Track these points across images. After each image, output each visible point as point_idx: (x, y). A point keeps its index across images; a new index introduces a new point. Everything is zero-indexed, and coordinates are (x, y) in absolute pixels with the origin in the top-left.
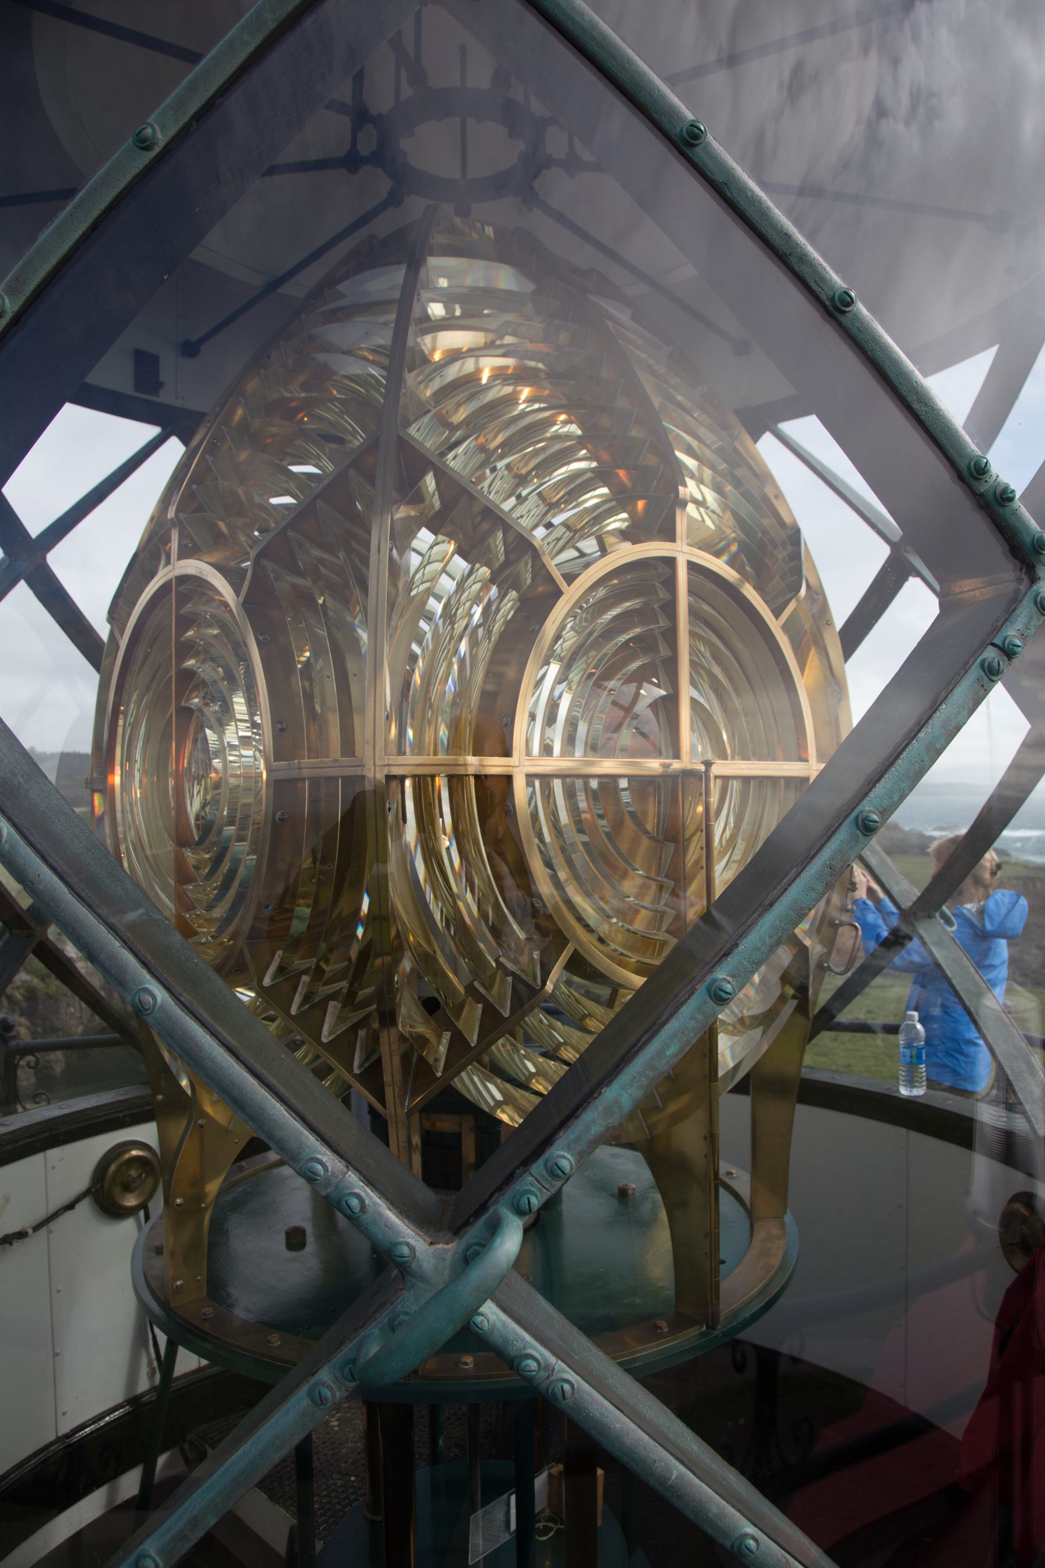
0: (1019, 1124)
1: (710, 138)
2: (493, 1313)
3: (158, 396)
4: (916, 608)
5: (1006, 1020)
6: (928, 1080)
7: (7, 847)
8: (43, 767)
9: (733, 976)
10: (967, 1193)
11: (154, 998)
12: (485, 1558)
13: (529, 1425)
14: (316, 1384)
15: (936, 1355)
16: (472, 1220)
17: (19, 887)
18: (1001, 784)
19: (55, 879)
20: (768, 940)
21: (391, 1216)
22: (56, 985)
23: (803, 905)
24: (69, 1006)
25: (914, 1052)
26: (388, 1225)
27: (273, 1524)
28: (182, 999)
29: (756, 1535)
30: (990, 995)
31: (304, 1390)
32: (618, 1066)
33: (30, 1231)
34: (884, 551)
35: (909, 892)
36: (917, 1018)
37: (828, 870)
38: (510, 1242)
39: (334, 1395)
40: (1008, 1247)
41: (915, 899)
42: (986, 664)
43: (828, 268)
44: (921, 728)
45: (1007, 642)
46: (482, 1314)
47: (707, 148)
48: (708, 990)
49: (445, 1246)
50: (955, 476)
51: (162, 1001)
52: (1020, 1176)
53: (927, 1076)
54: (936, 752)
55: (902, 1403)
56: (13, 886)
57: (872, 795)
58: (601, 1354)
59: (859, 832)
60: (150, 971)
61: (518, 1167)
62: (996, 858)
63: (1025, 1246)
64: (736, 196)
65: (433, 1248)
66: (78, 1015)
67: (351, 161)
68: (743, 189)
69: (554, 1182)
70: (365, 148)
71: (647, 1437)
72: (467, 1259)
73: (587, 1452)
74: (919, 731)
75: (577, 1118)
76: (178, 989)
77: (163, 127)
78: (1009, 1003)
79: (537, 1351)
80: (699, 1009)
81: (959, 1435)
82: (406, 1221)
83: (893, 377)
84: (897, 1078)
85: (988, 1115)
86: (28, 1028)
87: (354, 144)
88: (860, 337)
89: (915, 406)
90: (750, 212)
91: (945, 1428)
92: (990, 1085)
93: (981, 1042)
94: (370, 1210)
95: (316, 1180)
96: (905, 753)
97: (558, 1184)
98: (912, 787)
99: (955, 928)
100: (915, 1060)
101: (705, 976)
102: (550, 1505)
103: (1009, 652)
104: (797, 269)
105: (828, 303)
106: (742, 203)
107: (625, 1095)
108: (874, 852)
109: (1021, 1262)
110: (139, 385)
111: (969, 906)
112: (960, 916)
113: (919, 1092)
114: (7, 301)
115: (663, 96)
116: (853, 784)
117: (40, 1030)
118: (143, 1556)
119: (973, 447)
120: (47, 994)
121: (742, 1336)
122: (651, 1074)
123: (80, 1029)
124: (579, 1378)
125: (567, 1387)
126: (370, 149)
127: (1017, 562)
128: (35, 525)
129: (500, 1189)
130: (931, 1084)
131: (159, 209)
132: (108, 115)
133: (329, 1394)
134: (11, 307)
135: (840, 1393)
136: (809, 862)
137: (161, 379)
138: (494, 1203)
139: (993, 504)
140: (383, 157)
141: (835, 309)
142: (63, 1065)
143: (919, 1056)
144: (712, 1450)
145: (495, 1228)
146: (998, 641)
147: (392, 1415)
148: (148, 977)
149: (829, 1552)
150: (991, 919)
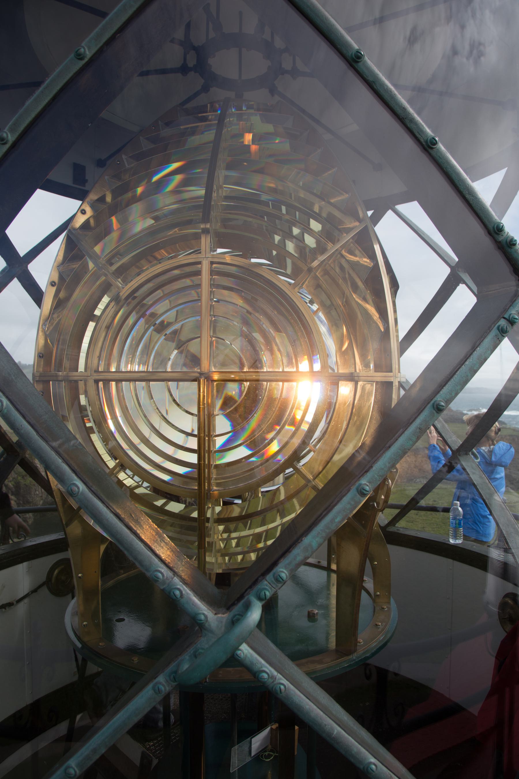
0: (510, 559)
1: (366, 58)
2: (246, 649)
3: (84, 186)
4: (463, 301)
6: (464, 535)
7: (5, 411)
8: (25, 371)
9: (370, 482)
10: (484, 592)
11: (78, 488)
13: (261, 704)
14: (156, 683)
15: (466, 673)
16: (236, 602)
17: (12, 431)
19: (29, 428)
21: (196, 600)
22: (29, 480)
23: (406, 447)
24: (36, 491)
25: (457, 522)
27: (134, 751)
28: (92, 489)
29: (376, 763)
30: (496, 494)
31: (151, 686)
33: (15, 603)
34: (447, 270)
35: (456, 442)
36: (459, 505)
37: (418, 430)
38: (255, 614)
39: (165, 689)
41: (459, 445)
42: (500, 328)
43: (425, 126)
46: (240, 650)
47: (365, 63)
48: (357, 489)
49: (223, 616)
50: (487, 233)
53: (463, 534)
54: (474, 372)
56: (6, 427)
57: (441, 392)
59: (434, 411)
61: (259, 577)
62: (498, 425)
63: (511, 620)
65: (216, 616)
66: (40, 495)
67: (184, 69)
68: (383, 85)
69: (278, 584)
70: (192, 62)
71: (322, 713)
72: (234, 622)
73: (290, 719)
74: (466, 361)
75: (290, 552)
76: (90, 484)
77: (89, 48)
78: (505, 498)
79: (268, 669)
81: (476, 713)
82: (203, 603)
83: (456, 181)
84: (448, 535)
85: (495, 554)
86: (15, 501)
87: (185, 59)
89: (467, 196)
90: (386, 96)
91: (471, 710)
95: (158, 581)
96: (458, 372)
97: (280, 585)
99: (479, 460)
100: (457, 526)
101: (356, 482)
103: (512, 322)
104: (409, 126)
105: (424, 144)
106: (382, 92)
107: (314, 541)
109: (509, 627)
110: (75, 181)
111: (483, 448)
112: (480, 453)
113: (459, 541)
115: (343, 37)
117: (21, 502)
118: (69, 767)
119: (496, 218)
120: (25, 484)
121: (369, 661)
122: (327, 531)
123: (41, 502)
124: (288, 683)
125: (282, 687)
126: (196, 62)
128: (22, 251)
129: (250, 587)
130: (466, 538)
131: (97, 78)
133: (163, 688)
135: (418, 691)
136: (409, 426)
137: (87, 178)
139: (505, 246)
140: (201, 67)
141: (428, 147)
142: (32, 520)
143: (460, 524)
144: (354, 720)
145: (248, 607)
146: (506, 316)
147: (192, 698)
148: (75, 477)
149: (412, 770)
150: (495, 455)
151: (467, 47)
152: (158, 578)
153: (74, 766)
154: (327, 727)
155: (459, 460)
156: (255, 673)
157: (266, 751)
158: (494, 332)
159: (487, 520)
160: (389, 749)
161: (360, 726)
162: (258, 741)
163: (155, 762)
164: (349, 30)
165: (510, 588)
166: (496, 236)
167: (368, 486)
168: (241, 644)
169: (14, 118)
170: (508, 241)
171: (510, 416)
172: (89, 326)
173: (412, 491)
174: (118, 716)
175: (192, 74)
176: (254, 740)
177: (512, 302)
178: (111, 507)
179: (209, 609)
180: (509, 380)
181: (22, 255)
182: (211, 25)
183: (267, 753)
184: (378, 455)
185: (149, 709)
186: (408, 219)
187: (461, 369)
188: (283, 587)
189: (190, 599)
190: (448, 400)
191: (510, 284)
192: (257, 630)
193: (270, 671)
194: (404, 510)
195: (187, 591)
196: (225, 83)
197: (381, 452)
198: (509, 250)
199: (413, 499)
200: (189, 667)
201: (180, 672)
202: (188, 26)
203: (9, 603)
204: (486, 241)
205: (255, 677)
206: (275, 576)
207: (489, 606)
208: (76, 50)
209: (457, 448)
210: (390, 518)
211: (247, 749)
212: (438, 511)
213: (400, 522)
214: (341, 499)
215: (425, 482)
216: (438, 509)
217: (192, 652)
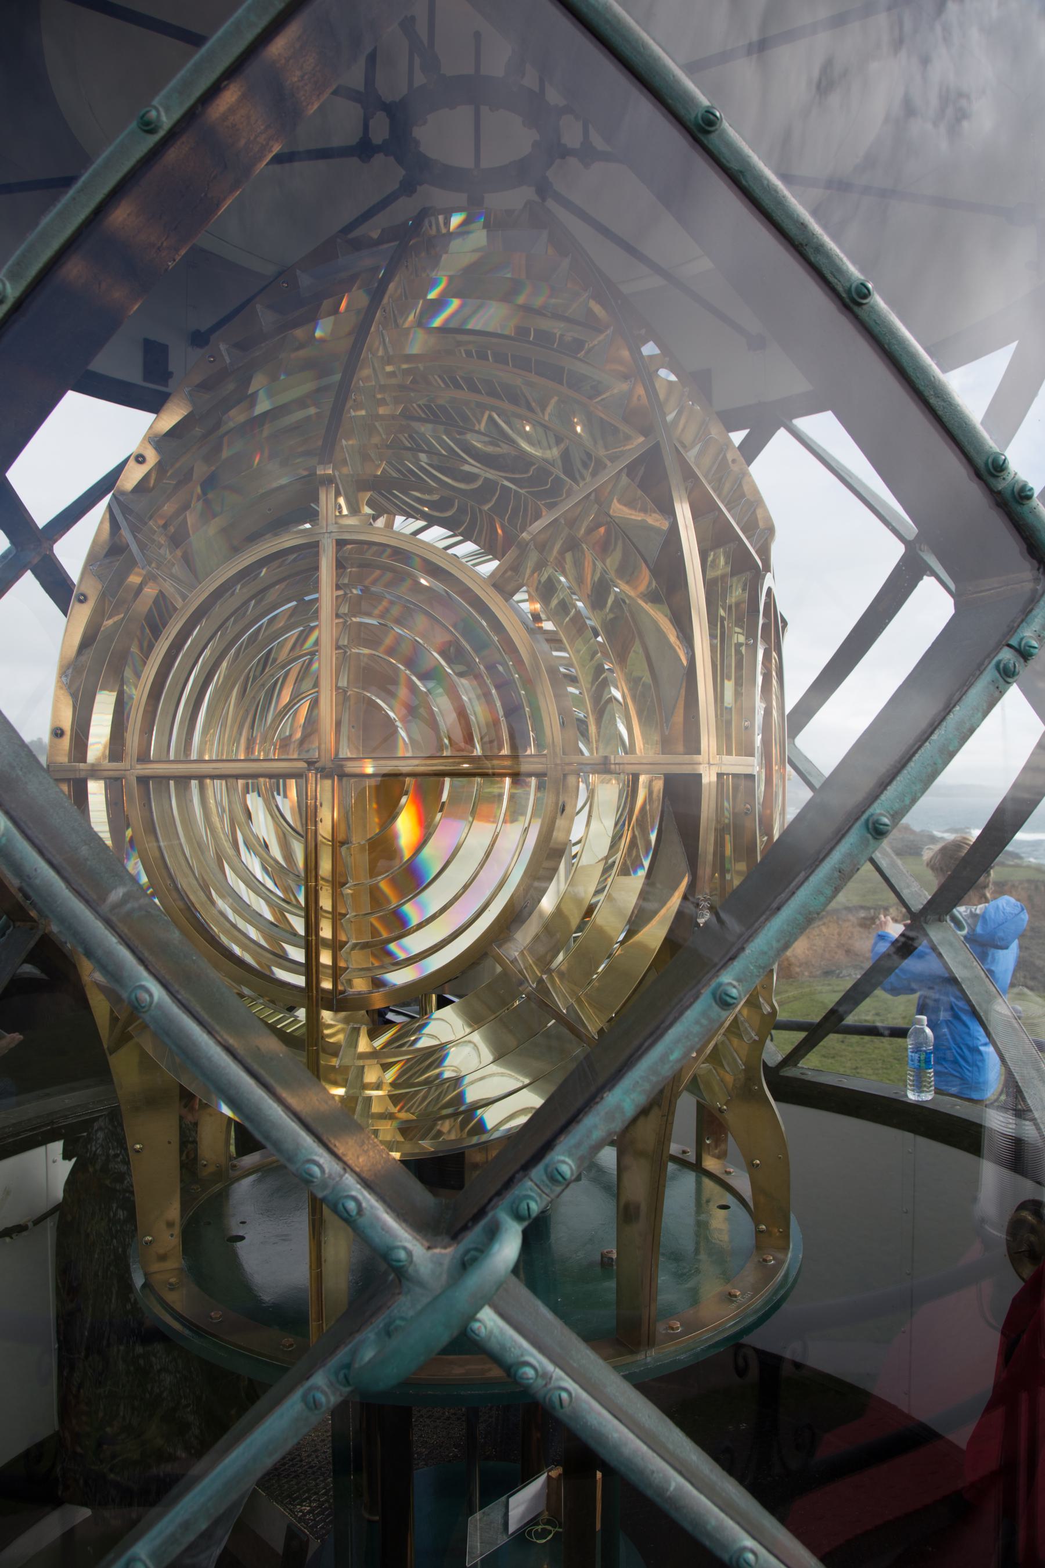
0: (1029, 1131)
3: (167, 386)
4: (931, 607)
5: (1016, 1025)
9: (739, 980)
10: (975, 1199)
11: (151, 995)
12: (482, 1560)
13: (524, 1430)
14: (311, 1389)
15: (942, 1365)
18: (1015, 786)
19: (51, 874)
20: (775, 944)
21: (389, 1220)
23: (811, 909)
25: (923, 1057)
26: (385, 1228)
28: (179, 997)
29: (755, 1549)
30: (1000, 1000)
31: (298, 1394)
32: (620, 1071)
33: (30, 1224)
34: (899, 549)
36: (926, 1023)
37: (837, 874)
38: (508, 1249)
39: (328, 1401)
40: (1015, 1256)
41: (925, 902)
42: (1001, 666)
43: (845, 259)
44: (934, 730)
45: (1023, 643)
48: (714, 994)
49: (443, 1251)
51: (159, 999)
52: (1029, 1184)
55: (906, 1411)
57: (883, 797)
58: (601, 1361)
59: (870, 836)
60: (147, 968)
61: (517, 1172)
63: (1033, 1255)
64: (751, 183)
67: (364, 149)
68: (759, 178)
69: (554, 1188)
71: (644, 1448)
72: (465, 1265)
73: (582, 1459)
74: (932, 733)
75: (578, 1122)
76: (176, 987)
77: (167, 110)
79: (535, 1358)
80: (704, 1014)
82: (404, 1225)
85: (998, 1122)
88: (877, 330)
89: (932, 401)
90: (767, 202)
91: (951, 1437)
92: (999, 1090)
93: (990, 1049)
94: (367, 1213)
96: (917, 755)
97: (559, 1189)
98: (923, 791)
100: (923, 1065)
101: (710, 979)
102: (548, 1509)
103: (1025, 654)
104: (813, 259)
105: (844, 295)
106: (758, 192)
108: (885, 854)
109: (1028, 1271)
110: (148, 375)
113: (927, 1097)
114: (8, 285)
115: (677, 81)
116: (866, 783)
118: (133, 1559)
121: (746, 1340)
122: (654, 1079)
124: (576, 1386)
125: (564, 1395)
126: (387, 136)
127: (1035, 562)
128: (42, 515)
129: (499, 1193)
130: (938, 1091)
132: (115, 101)
133: (323, 1399)
134: (12, 292)
135: (843, 1398)
136: (817, 866)
137: (171, 369)
138: (493, 1208)
139: (1011, 503)
140: (400, 144)
141: (851, 301)
143: (927, 1061)
145: (493, 1233)
146: (1014, 642)
147: (378, 1435)
148: (144, 974)
151: (934, 101)
152: (311, 1175)
153: (143, 1556)
154: (655, 1475)
155: (924, 930)
156: (510, 1370)
157: (537, 1524)
158: (990, 674)
159: (979, 1057)
160: (783, 1520)
161: (724, 1473)
162: (522, 1503)
163: (314, 1545)
164: (692, 68)
165: (1028, 1189)
166: (992, 481)
167: (735, 987)
168: (481, 1308)
169: (18, 252)
170: (1016, 489)
171: (1022, 843)
172: (96, 705)
173: (829, 995)
174: (227, 1461)
175: (379, 159)
176: (513, 1501)
177: (1026, 613)
178: (217, 1032)
179: (415, 1238)
180: (1026, 769)
181: (40, 526)
182: (417, 61)
183: (539, 1528)
184: (757, 925)
185: (295, 1441)
186: (819, 446)
187: (923, 750)
188: (565, 1193)
189: (378, 1218)
190: (896, 813)
191: (1023, 574)
192: (514, 1279)
193: (540, 1363)
194: (814, 1034)
195: (369, 1201)
196: (450, 177)
197: (762, 919)
198: (1019, 508)
199: (833, 1012)
200: (374, 1357)
201: (357, 1366)
202: (372, 58)
203: (19, 1226)
204: (973, 491)
205: (509, 1375)
206: (549, 1170)
207: (987, 1227)
208: (143, 112)
209: (921, 907)
210: (789, 1049)
211: (498, 1518)
212: (881, 1035)
213: (807, 1057)
214: (681, 1014)
215: (859, 977)
216: (882, 1031)
217: (381, 1325)
